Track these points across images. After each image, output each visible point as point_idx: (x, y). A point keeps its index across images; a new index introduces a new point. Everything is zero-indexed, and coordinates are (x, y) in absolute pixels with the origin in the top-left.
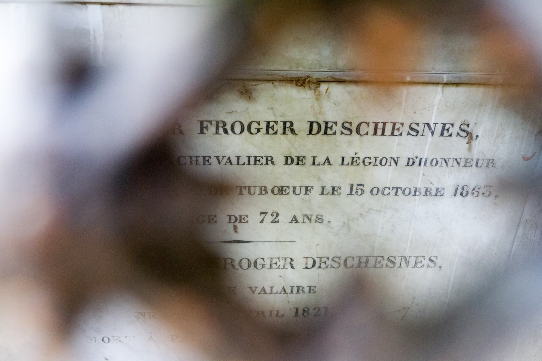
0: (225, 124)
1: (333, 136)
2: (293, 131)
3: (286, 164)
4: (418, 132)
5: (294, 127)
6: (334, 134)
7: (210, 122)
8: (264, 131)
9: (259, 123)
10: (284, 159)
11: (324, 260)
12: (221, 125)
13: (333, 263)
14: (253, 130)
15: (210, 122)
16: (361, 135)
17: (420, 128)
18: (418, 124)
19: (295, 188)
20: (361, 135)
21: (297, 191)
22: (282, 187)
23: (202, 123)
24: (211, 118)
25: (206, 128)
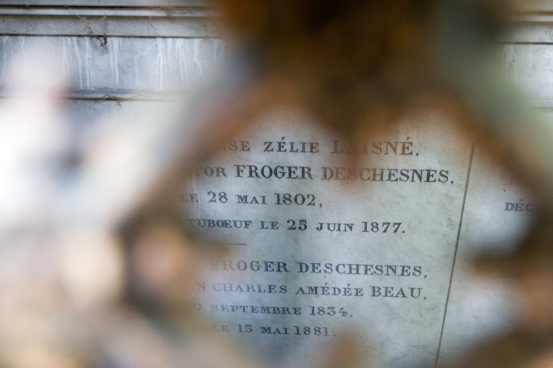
0: (256, 169)
1: (434, 183)
2: (310, 176)
3: (507, 209)
4: (408, 177)
5: (311, 173)
6: (435, 181)
7: (244, 166)
8: (287, 175)
9: (282, 168)
10: (505, 205)
11: (269, 264)
12: (220, 170)
13: (377, 271)
14: (280, 175)
15: (244, 166)
16: (363, 180)
17: (410, 174)
18: (407, 171)
19: (235, 222)
20: (363, 180)
21: (332, 228)
22: (226, 221)
23: (238, 167)
24: (246, 163)
25: (242, 171)
